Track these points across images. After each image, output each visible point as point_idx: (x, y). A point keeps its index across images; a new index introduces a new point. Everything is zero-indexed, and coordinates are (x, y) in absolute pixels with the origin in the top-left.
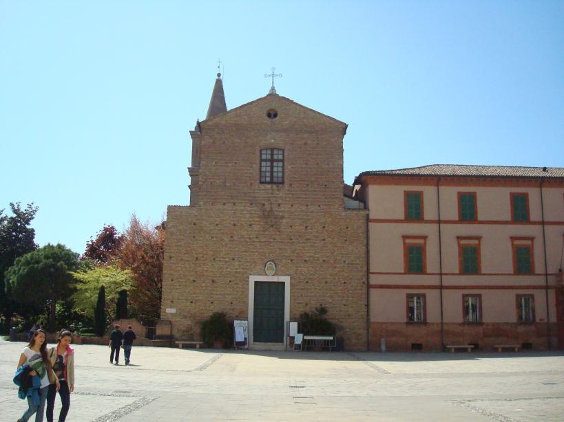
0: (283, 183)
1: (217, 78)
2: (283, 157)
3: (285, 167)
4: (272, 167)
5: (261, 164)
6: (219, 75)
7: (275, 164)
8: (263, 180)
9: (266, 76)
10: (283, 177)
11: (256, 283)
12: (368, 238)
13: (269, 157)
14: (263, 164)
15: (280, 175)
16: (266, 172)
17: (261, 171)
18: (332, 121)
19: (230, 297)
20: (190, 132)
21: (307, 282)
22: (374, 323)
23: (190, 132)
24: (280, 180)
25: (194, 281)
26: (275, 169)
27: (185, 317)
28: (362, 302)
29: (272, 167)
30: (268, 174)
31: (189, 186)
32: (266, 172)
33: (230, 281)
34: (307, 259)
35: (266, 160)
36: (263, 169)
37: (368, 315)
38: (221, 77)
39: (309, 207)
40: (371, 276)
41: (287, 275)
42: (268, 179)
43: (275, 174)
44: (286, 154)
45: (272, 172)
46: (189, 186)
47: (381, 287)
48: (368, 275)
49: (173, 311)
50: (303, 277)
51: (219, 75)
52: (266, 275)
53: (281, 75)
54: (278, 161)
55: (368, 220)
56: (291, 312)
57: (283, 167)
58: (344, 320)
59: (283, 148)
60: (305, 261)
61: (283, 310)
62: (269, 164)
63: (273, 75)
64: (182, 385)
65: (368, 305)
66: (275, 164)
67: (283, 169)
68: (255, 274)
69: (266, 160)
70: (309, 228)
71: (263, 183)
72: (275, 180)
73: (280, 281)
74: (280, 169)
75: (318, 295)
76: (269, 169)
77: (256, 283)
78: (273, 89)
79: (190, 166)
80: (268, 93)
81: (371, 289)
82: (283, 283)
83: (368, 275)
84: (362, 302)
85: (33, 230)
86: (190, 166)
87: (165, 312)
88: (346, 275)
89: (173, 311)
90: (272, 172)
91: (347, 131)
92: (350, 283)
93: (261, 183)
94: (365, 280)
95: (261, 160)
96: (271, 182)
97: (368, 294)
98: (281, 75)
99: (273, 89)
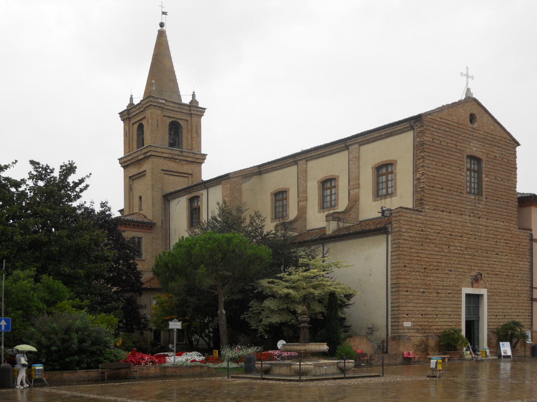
1: (159, 28)
6: (162, 25)
41: (486, 288)
44: (483, 165)
51: (162, 25)
55: (532, 240)
78: (468, 90)
99: (468, 90)
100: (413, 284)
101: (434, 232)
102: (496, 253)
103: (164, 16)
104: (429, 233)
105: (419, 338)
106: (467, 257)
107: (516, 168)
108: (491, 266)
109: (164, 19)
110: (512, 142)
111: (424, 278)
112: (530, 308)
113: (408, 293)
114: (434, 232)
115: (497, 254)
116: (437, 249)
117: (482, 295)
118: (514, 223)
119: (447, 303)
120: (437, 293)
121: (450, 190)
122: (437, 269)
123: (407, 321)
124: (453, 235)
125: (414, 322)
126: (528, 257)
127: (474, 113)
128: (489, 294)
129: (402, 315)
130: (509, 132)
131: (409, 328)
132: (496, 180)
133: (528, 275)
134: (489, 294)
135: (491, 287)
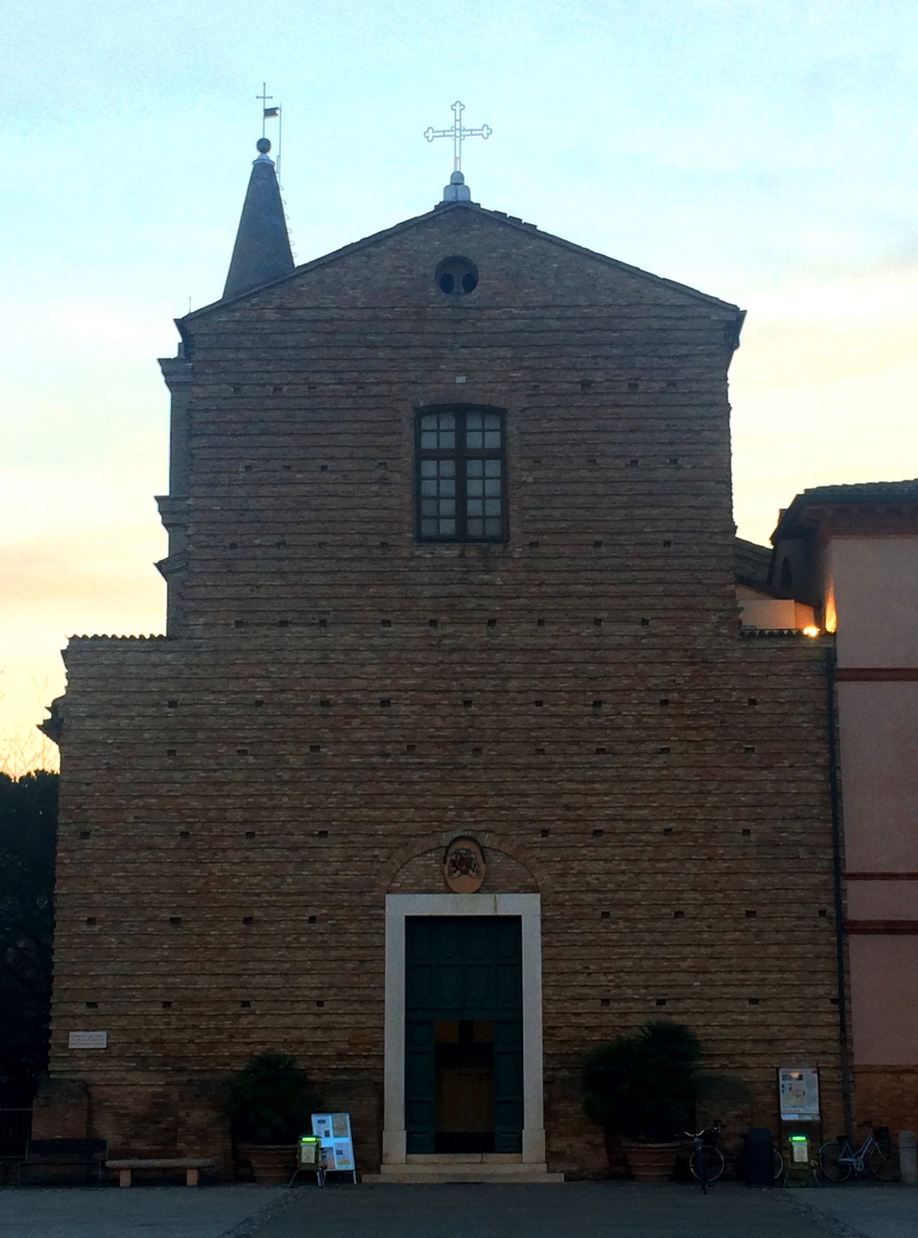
0: (504, 538)
1: (256, 154)
2: (504, 438)
3: (513, 476)
4: (461, 478)
5: (418, 468)
6: (264, 146)
7: (474, 467)
8: (428, 529)
9: (431, 134)
10: (504, 517)
11: (411, 921)
12: (832, 739)
13: (449, 441)
14: (429, 468)
15: (494, 508)
16: (438, 498)
17: (418, 496)
18: (681, 300)
19: (314, 981)
20: (162, 361)
21: (606, 915)
22: (871, 1070)
23: (162, 361)
24: (493, 528)
25: (175, 921)
26: (474, 488)
27: (144, 1063)
28: (821, 991)
29: (461, 478)
30: (448, 507)
31: (160, 566)
32: (438, 498)
33: (312, 920)
34: (602, 826)
35: (438, 455)
36: (429, 488)
37: (844, 1039)
38: (272, 155)
39: (606, 628)
40: (852, 887)
41: (534, 890)
42: (448, 527)
43: (473, 507)
44: (511, 429)
45: (461, 497)
46: (160, 566)
47: (893, 928)
48: (837, 883)
49: (96, 1040)
50: (589, 898)
51: (264, 146)
52: (451, 891)
53: (485, 132)
54: (485, 455)
56: (548, 1032)
57: (504, 477)
58: (750, 1062)
59: (499, 403)
60: (598, 833)
61: (518, 1022)
62: (448, 467)
63: (458, 132)
64: (449, 1164)
65: (841, 1001)
66: (474, 467)
67: (505, 486)
68: (402, 890)
69: (438, 455)
70: (606, 708)
71: (431, 540)
72: (474, 528)
73: (501, 913)
74: (493, 487)
75: (646, 964)
76: (448, 487)
77: (411, 921)
78: (457, 180)
79: (165, 492)
80: (439, 198)
81: (854, 940)
82: (516, 921)
83: (837, 883)
84: (821, 991)
85: (50, 728)
86: (165, 492)
87: (65, 1046)
88: (753, 882)
89: (96, 1040)
90: (461, 497)
91: (743, 336)
92: (769, 918)
93: (421, 539)
94: (826, 899)
95: (421, 455)
96: (461, 537)
97: (841, 957)
98: (485, 132)
99: (457, 180)
100: (119, 894)
101: (229, 704)
102: (594, 747)
103: (271, 120)
104: (207, 709)
105: (150, 1090)
106: (415, 776)
107: (728, 408)
108: (565, 799)
109: (271, 132)
110: (704, 311)
111: (177, 868)
112: (833, 965)
113: (97, 928)
114: (229, 704)
115: (600, 751)
116: (251, 759)
117: (516, 921)
118: (714, 619)
119: (300, 955)
120: (247, 920)
121: (320, 544)
122: (250, 835)
123: (88, 1030)
124: (336, 704)
125: (124, 1030)
126: (816, 747)
127: (459, 253)
128: (376, 939)
129: (63, 1006)
130: (664, 279)
131: (91, 1054)
132: (592, 470)
133: (818, 824)
134: (376, 939)
135: (565, 884)
